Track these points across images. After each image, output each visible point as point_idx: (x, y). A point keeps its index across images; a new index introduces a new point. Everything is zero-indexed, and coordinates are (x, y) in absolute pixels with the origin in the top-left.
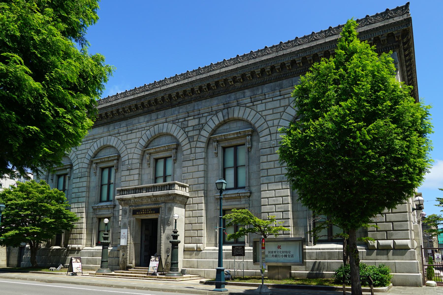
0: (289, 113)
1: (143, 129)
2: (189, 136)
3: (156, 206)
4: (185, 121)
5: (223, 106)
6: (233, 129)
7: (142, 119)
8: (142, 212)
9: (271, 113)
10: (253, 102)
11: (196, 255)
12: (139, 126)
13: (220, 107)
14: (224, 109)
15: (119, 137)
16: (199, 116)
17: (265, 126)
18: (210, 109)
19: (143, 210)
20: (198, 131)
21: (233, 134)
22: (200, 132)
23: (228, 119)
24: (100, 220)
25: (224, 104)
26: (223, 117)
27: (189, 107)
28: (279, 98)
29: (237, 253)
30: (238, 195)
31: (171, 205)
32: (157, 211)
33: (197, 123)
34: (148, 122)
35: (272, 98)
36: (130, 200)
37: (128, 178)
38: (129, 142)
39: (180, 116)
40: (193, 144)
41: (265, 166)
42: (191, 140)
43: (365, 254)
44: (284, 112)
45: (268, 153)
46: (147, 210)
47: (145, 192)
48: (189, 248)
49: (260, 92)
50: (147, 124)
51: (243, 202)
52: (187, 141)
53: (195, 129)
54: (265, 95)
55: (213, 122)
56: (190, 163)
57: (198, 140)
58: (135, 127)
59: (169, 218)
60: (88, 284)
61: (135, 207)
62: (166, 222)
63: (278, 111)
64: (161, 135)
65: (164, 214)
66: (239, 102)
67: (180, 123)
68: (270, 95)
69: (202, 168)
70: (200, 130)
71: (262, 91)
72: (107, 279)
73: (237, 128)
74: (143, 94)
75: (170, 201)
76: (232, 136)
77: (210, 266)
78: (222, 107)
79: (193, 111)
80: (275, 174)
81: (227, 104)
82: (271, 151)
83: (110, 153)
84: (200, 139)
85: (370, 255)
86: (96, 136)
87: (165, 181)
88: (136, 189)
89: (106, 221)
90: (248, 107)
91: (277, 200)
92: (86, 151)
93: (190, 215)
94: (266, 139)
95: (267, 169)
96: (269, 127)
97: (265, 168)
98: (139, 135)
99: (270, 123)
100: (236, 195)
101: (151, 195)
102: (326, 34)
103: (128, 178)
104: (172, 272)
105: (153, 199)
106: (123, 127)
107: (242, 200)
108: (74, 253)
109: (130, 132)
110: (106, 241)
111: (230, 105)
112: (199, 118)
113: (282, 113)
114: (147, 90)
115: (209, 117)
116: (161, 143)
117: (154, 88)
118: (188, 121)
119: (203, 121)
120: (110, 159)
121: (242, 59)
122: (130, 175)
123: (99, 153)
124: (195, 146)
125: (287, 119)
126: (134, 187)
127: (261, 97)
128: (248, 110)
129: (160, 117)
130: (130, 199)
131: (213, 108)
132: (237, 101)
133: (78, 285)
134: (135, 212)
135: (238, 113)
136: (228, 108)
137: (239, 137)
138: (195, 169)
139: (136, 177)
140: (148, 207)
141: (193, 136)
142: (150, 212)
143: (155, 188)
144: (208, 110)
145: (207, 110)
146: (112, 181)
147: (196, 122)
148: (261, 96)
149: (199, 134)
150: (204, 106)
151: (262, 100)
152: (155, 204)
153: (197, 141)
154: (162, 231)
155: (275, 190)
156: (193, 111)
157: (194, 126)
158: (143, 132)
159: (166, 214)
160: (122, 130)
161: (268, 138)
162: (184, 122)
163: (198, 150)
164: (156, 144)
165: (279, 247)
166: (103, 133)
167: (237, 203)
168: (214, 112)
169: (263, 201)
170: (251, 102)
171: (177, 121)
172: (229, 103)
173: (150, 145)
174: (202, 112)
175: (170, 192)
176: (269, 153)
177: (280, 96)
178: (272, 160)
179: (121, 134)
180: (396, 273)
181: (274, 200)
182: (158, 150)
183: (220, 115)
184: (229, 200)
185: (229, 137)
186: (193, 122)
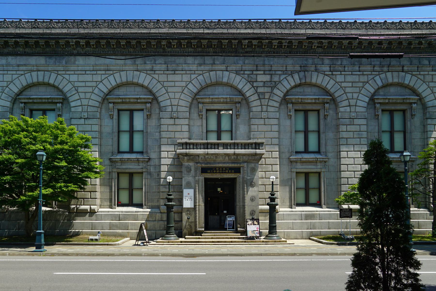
0: (368, 89)
1: (193, 72)
2: (258, 91)
3: (236, 165)
4: (252, 74)
5: (299, 68)
6: (307, 93)
7: (190, 60)
9: (351, 86)
10: (332, 71)
11: (89, 216)
12: (186, 68)
13: (296, 68)
14: (300, 71)
15: (154, 76)
16: (271, 72)
17: (344, 97)
18: (285, 68)
20: (270, 88)
21: (312, 99)
22: (272, 90)
23: (305, 83)
25: (301, 66)
26: (300, 79)
27: (258, 60)
28: (358, 73)
29: (345, 216)
30: (316, 159)
31: (255, 166)
32: (237, 170)
33: (268, 80)
34: (200, 65)
35: (352, 71)
37: (171, 128)
38: (172, 84)
39: (247, 68)
40: (265, 102)
41: (344, 135)
42: (261, 97)
43: (428, 215)
44: (363, 87)
45: (348, 124)
46: (222, 168)
47: (222, 148)
48: (264, 210)
49: (339, 63)
51: (319, 167)
52: (256, 97)
53: (266, 85)
54: (345, 67)
55: (288, 83)
56: (262, 122)
57: (271, 98)
58: (180, 68)
59: (253, 179)
61: (205, 164)
62: (249, 183)
63: (358, 86)
64: (218, 84)
65: (246, 174)
66: (317, 68)
67: (246, 76)
68: (350, 68)
69: (275, 128)
70: (273, 88)
71: (342, 63)
72: (259, 247)
73: (312, 94)
75: (254, 161)
76: (309, 101)
77: (290, 227)
78: (298, 68)
79: (264, 65)
80: (354, 143)
81: (304, 66)
82: (351, 121)
83: (136, 93)
84: (273, 97)
86: (112, 68)
87: (219, 138)
88: (186, 144)
90: (326, 75)
91: (356, 167)
92: (94, 84)
93: (262, 176)
94: (346, 110)
95: (347, 138)
96: (348, 99)
97: (345, 137)
98: (186, 78)
99: (350, 95)
100: (314, 159)
101: (233, 152)
102: (411, 26)
103: (171, 128)
104: (168, 236)
105: (233, 157)
106: (160, 63)
107: (318, 164)
109: (173, 72)
110: (273, 203)
111: (308, 69)
112: (271, 75)
113: (361, 88)
114: (208, 28)
115: (283, 76)
116: (216, 93)
117: (218, 28)
118: (257, 75)
119: (276, 78)
120: (139, 101)
121: (331, 26)
122: (174, 124)
123: (116, 90)
124: (266, 104)
125: (365, 94)
127: (340, 68)
128: (327, 78)
129: (218, 63)
130: (198, 155)
131: (287, 68)
132: (316, 67)
133: (243, 257)
134: (204, 170)
135: (317, 79)
136: (305, 71)
137: (315, 103)
138: (268, 128)
139: (186, 128)
140: (225, 165)
141: (264, 93)
142: (227, 171)
144: (281, 68)
145: (281, 68)
146: (301, 136)
147: (267, 78)
148: (341, 67)
149: (271, 92)
150: (277, 63)
151: (341, 71)
153: (269, 99)
154: (246, 193)
155: (168, 152)
156: (264, 65)
157: (264, 82)
158: (193, 76)
159: (249, 175)
160: (158, 67)
161: (348, 109)
162: (251, 76)
163: (270, 109)
164: (209, 93)
166: (125, 65)
168: (290, 72)
169: (343, 168)
170: (330, 71)
171: (242, 72)
172: (306, 66)
173: (24, 93)
174: (274, 68)
175: (258, 151)
176: (348, 123)
177: (359, 71)
178: (351, 130)
179: (157, 72)
180: (311, 229)
181: (353, 167)
183: (296, 76)
184: (305, 164)
185: (306, 101)
186: (262, 78)
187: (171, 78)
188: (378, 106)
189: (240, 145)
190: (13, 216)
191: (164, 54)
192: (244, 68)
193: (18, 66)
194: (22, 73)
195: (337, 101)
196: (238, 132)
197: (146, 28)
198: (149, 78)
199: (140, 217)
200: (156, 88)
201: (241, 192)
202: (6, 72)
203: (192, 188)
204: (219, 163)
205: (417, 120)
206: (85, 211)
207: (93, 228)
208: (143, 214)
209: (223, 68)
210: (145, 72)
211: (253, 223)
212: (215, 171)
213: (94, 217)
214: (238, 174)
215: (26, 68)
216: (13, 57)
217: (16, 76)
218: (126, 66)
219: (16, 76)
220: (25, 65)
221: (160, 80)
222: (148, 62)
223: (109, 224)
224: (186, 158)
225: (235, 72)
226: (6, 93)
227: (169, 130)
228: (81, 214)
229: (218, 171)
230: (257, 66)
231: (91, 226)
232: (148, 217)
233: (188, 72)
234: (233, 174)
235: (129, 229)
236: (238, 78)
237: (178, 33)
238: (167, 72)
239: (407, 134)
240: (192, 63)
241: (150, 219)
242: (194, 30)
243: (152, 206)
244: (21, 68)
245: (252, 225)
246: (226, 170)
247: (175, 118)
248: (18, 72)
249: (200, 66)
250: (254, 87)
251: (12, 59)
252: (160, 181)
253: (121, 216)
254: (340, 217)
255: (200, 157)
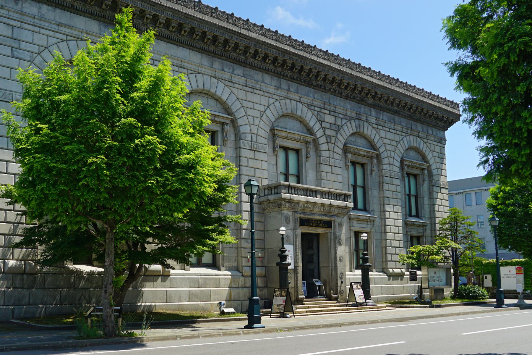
2: (326, 133)
5: (355, 115)
6: (358, 144)
7: (267, 78)
8: (313, 223)
11: (162, 281)
12: (264, 89)
14: (356, 119)
19: (314, 221)
24: (357, 234)
25: (356, 114)
36: (299, 203)
46: (318, 221)
50: (276, 91)
51: (369, 226)
60: (331, 326)
73: (361, 145)
74: (287, 48)
76: (362, 153)
78: (354, 115)
79: (330, 104)
85: (165, 281)
86: (186, 65)
89: (364, 236)
103: (252, 163)
108: (398, 280)
109: (251, 90)
126: (328, 190)
130: (298, 203)
134: (303, 222)
135: (368, 131)
143: (330, 195)
144: (342, 111)
152: (326, 215)
158: (271, 101)
165: (435, 273)
167: (365, 226)
171: (313, 108)
174: (338, 110)
182: (291, 135)
186: (330, 119)
187: (250, 97)
188: (406, 167)
189: (333, 195)
190: (49, 279)
191: (244, 64)
192: (314, 102)
193: (59, 24)
194: (64, 37)
195: (381, 157)
196: (308, 179)
197: (236, 25)
198: (227, 91)
199: (222, 282)
200: (235, 107)
201: (333, 251)
202: (37, 29)
203: (291, 244)
204: (315, 214)
205: (426, 185)
206: (155, 274)
207: (168, 301)
208: (225, 278)
209: (297, 98)
210: (223, 81)
211: (281, 293)
212: (311, 224)
213: (168, 283)
214: (329, 230)
215: (71, 31)
216: (50, 8)
217: (54, 41)
218: (202, 67)
219: (54, 41)
220: (70, 27)
221: (239, 97)
222: (226, 69)
223: (187, 292)
224: (287, 204)
225: (307, 105)
226: (37, 64)
227: (250, 165)
228: (151, 278)
229: (314, 224)
230: (324, 104)
231: (165, 297)
232: (231, 283)
233: (266, 94)
234: (325, 229)
235: (212, 299)
236: (310, 114)
237: (268, 43)
238: (246, 89)
239: (419, 199)
240: (269, 83)
241: (233, 285)
242: (281, 44)
243: (229, 267)
244: (62, 29)
245: (279, 298)
246: (321, 223)
247: (255, 151)
248: (57, 35)
249: (277, 89)
250: (322, 127)
251: (48, 10)
252: (241, 233)
253: (200, 281)
254: (410, 280)
255: (300, 205)
